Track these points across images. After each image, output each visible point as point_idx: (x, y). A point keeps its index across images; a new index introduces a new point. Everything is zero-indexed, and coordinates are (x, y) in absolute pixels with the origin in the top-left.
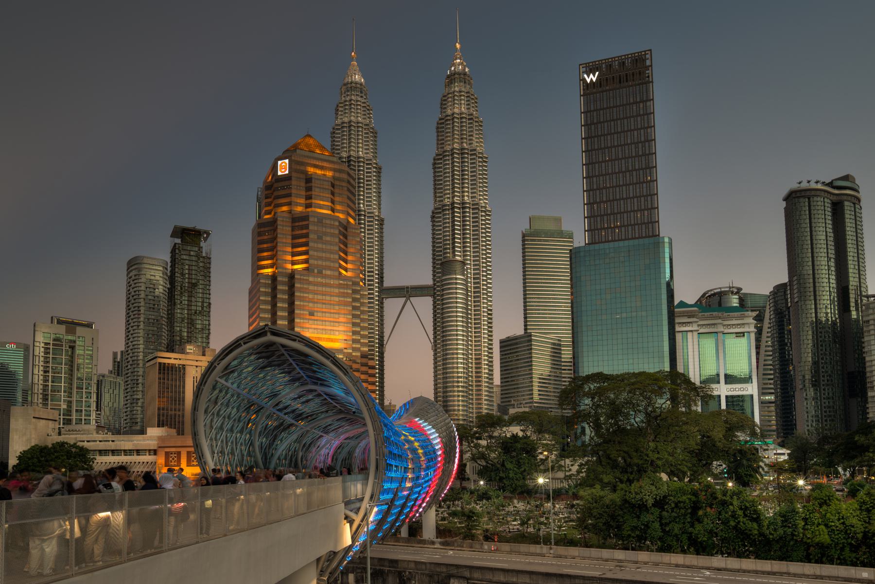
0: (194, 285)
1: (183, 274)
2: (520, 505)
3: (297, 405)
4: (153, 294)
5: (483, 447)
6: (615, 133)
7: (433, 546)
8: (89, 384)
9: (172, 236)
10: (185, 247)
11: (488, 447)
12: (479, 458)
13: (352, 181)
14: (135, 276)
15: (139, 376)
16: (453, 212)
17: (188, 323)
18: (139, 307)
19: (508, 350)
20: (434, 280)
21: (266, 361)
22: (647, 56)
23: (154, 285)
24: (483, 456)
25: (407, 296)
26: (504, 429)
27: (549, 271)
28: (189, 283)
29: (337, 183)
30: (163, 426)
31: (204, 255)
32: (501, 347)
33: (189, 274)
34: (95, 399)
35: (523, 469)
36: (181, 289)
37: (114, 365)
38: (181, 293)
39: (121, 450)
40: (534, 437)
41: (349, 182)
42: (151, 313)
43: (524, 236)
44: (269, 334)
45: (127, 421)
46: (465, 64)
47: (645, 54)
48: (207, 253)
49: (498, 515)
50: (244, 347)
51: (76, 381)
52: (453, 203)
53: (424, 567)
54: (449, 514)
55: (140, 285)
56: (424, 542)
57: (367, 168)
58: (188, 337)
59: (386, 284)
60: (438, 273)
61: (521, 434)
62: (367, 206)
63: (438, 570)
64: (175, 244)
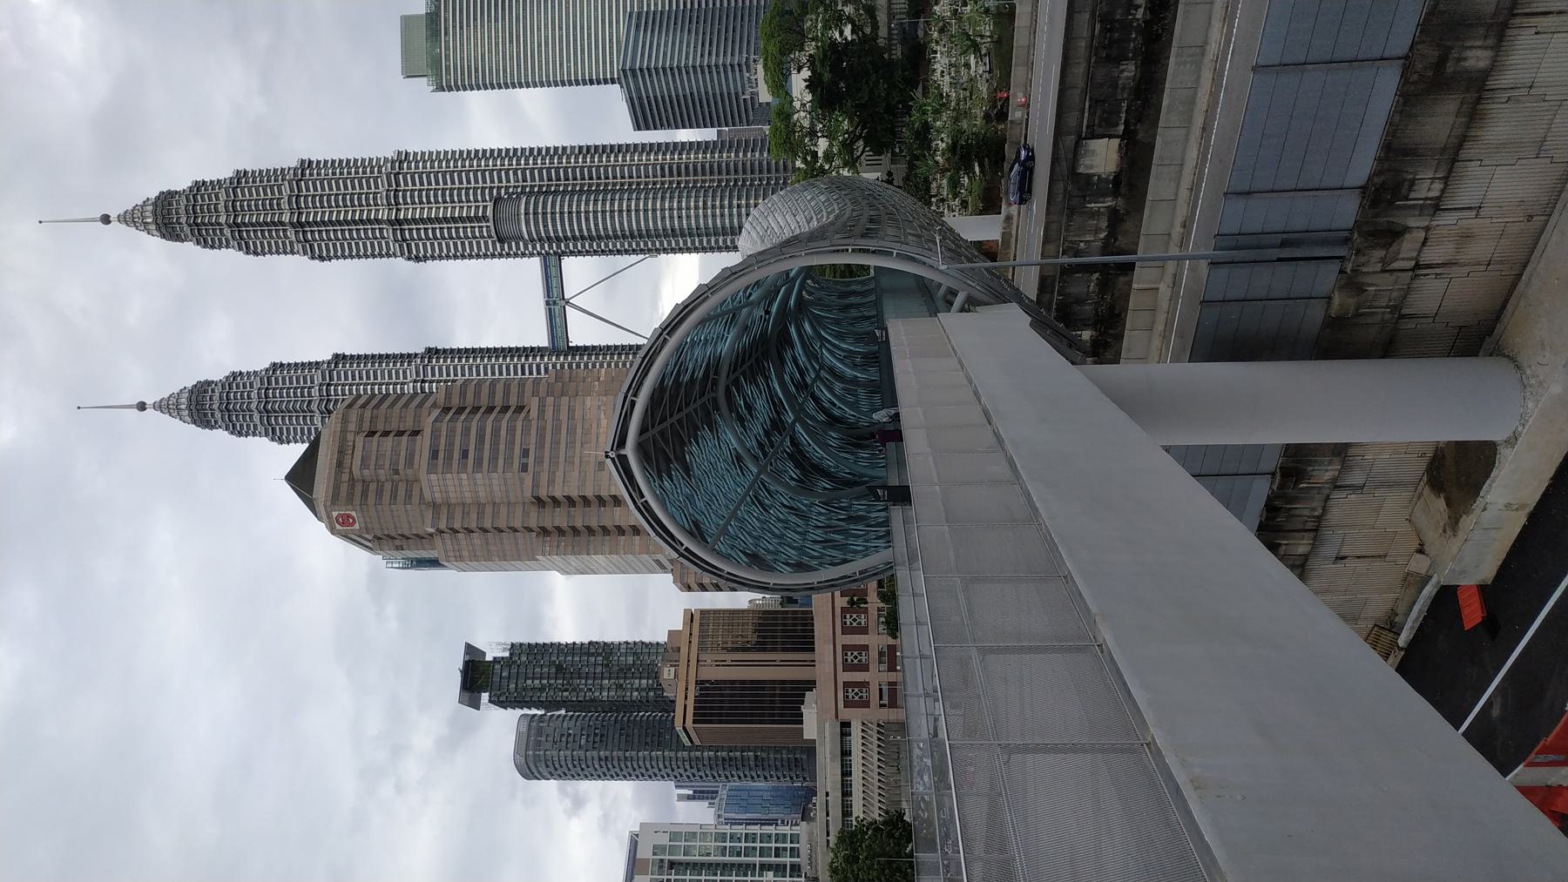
0: (559, 668)
1: (542, 689)
2: (940, 62)
3: (757, 429)
4: (577, 738)
5: (831, 145)
7: (1015, 218)
8: (731, 838)
9: (478, 708)
10: (496, 686)
11: (830, 136)
12: (852, 152)
13: (361, 402)
14: (548, 766)
16: (406, 221)
17: (625, 678)
18: (600, 759)
19: (652, 114)
20: (532, 255)
21: (675, 465)
23: (562, 735)
24: (848, 146)
25: (563, 303)
26: (797, 105)
27: (496, 10)
28: (556, 679)
29: (366, 427)
30: (801, 715)
31: (507, 654)
32: (648, 128)
33: (541, 678)
34: (758, 827)
35: (870, 67)
36: (566, 690)
37: (699, 798)
38: (574, 690)
39: (842, 781)
40: (811, 48)
41: (364, 406)
42: (610, 739)
43: (440, 88)
44: (622, 452)
48: (504, 650)
49: (958, 101)
50: (648, 497)
51: (727, 858)
52: (390, 222)
53: (1054, 226)
54: (955, 196)
55: (562, 758)
56: (1006, 236)
57: (277, 383)
58: (648, 678)
59: (543, 341)
60: (518, 248)
61: (806, 73)
62: (405, 378)
63: (1060, 198)
64: (490, 701)
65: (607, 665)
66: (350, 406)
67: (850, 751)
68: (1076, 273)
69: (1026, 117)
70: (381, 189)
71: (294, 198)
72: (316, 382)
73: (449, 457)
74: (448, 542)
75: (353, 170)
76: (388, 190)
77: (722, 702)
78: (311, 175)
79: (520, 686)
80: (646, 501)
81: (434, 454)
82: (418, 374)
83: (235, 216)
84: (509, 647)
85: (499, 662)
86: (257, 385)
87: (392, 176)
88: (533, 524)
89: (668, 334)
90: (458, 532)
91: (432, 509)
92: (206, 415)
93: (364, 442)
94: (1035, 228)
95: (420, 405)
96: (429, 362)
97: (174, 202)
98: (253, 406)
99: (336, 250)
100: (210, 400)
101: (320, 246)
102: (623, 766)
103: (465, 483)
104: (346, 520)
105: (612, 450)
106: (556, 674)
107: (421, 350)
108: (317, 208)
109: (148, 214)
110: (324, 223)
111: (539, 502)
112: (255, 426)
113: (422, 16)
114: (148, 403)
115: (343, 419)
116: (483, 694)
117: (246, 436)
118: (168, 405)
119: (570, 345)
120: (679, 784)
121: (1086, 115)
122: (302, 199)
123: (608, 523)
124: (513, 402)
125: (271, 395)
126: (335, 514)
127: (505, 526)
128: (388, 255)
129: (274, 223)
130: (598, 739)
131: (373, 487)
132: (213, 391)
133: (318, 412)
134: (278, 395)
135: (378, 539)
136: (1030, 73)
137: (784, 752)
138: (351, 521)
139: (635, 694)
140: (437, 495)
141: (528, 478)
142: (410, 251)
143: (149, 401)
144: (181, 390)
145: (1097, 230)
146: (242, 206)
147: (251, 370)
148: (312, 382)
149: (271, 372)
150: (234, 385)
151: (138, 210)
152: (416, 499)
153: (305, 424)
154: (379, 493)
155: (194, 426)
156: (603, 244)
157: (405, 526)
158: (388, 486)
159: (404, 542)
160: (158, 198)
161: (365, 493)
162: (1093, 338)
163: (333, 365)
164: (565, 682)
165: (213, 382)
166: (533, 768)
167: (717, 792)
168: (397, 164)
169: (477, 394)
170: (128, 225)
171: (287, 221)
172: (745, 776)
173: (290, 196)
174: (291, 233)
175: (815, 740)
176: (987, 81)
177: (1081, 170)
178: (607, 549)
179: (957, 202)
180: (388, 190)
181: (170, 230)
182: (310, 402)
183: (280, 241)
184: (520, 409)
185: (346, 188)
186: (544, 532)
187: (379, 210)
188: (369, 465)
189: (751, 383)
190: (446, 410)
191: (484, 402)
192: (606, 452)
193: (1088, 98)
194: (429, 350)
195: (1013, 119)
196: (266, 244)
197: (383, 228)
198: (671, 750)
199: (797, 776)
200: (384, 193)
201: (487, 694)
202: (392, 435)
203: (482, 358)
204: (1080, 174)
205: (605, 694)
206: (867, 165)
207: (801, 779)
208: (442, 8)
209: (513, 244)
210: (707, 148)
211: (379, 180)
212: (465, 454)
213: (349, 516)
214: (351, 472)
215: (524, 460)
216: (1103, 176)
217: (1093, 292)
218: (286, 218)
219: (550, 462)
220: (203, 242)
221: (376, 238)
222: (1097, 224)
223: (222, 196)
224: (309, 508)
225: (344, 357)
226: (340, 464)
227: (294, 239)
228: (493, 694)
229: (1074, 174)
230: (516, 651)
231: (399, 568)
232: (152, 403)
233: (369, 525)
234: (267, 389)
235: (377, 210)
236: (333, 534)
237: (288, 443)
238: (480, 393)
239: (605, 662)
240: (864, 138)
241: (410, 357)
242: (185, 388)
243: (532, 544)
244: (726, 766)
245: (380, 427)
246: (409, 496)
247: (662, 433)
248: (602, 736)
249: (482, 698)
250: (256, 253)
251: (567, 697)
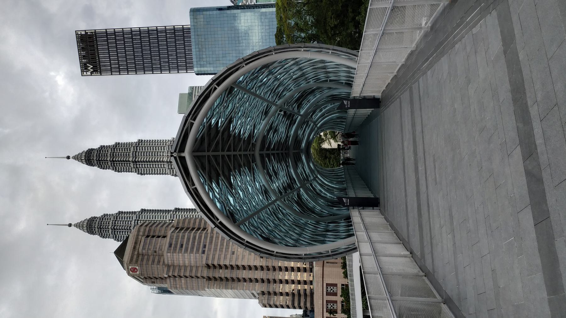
6: (125, 53)
13: (145, 224)
22: (79, 33)
29: (146, 233)
41: (146, 226)
44: (183, 155)
47: (78, 34)
57: (119, 219)
66: (141, 225)
70: (165, 150)
71: (135, 152)
72: (134, 219)
73: (176, 247)
74: (172, 281)
75: (162, 143)
76: (168, 151)
78: (142, 145)
81: (170, 245)
82: (171, 218)
86: (112, 219)
87: (135, 147)
88: (205, 275)
90: (182, 277)
91: (167, 267)
92: (92, 229)
93: (145, 239)
95: (167, 226)
96: (175, 213)
97: (93, 153)
98: (110, 227)
99: (147, 171)
100: (95, 224)
101: (141, 169)
103: (180, 257)
104: (134, 270)
105: (175, 151)
107: (173, 209)
108: (142, 156)
109: (83, 156)
110: (160, 161)
111: (214, 267)
112: (109, 235)
113: (187, 93)
114: (72, 224)
117: (106, 238)
118: (80, 225)
122: (137, 153)
123: (240, 277)
124: (202, 226)
125: (117, 223)
126: (130, 267)
127: (194, 275)
128: (165, 174)
129: (126, 161)
131: (146, 257)
132: (96, 221)
133: (110, 229)
134: (119, 223)
135: (146, 279)
138: (136, 270)
140: (170, 262)
141: (205, 256)
143: (73, 224)
144: (85, 220)
146: (116, 155)
147: (111, 213)
148: (132, 219)
149: (118, 215)
151: (80, 155)
152: (161, 263)
153: (123, 234)
154: (148, 260)
155: (87, 233)
157: (156, 273)
158: (151, 258)
159: (155, 280)
160: (87, 151)
161: (142, 260)
163: (140, 213)
165: (97, 217)
168: (172, 142)
169: (189, 222)
170: (75, 160)
171: (131, 160)
173: (133, 152)
174: (132, 165)
178: (230, 287)
181: (90, 162)
182: (130, 226)
183: (122, 167)
184: (204, 229)
185: (153, 149)
186: (209, 279)
187: (164, 158)
188: (145, 249)
190: (177, 228)
191: (191, 226)
194: (176, 209)
196: (122, 168)
197: (165, 164)
200: (167, 152)
202: (161, 237)
203: (192, 212)
208: (194, 91)
211: (165, 147)
212: (182, 246)
213: (136, 268)
214: (138, 251)
215: (204, 249)
218: (130, 159)
219: (225, 251)
220: (101, 167)
221: (148, 168)
223: (132, 149)
224: (121, 265)
225: (145, 210)
226: (134, 248)
227: (133, 167)
231: (156, 293)
232: (74, 224)
233: (143, 273)
234: (116, 221)
235: (163, 158)
236: (129, 275)
238: (190, 222)
241: (169, 211)
242: (86, 219)
243: (204, 283)
245: (152, 234)
246: (159, 262)
250: (119, 172)
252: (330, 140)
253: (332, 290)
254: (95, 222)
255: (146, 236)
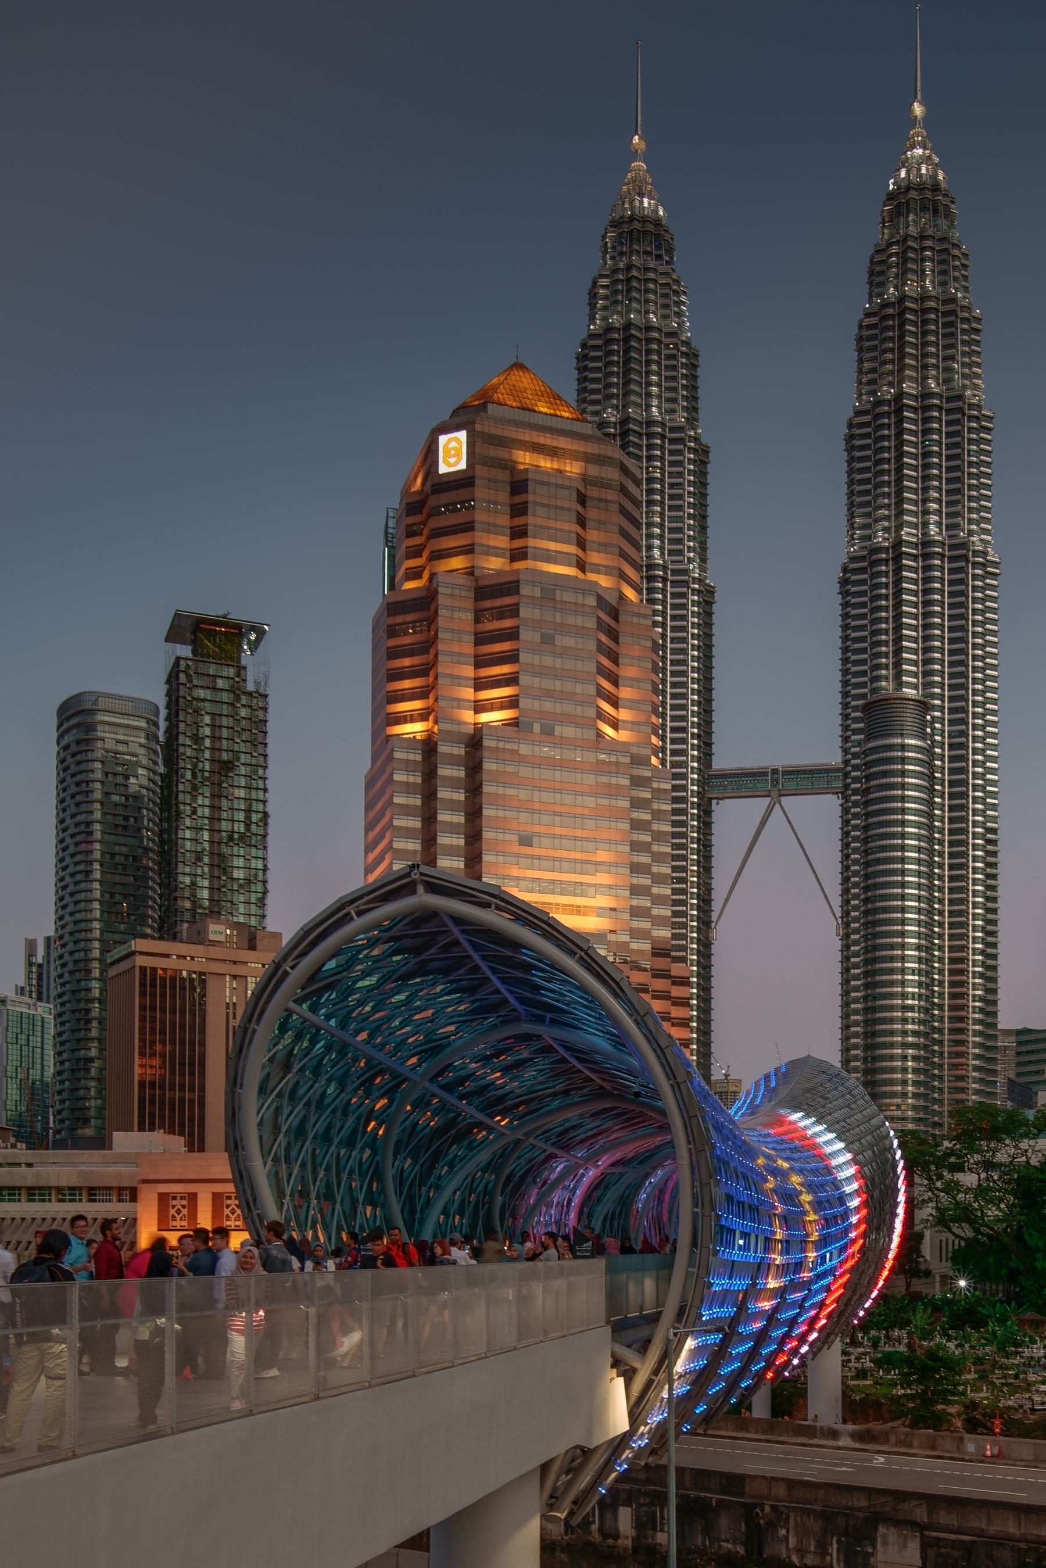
1: (197, 739)
7: (832, 1443)
9: (168, 639)
11: (980, 1191)
15: (92, 1000)
20: (845, 751)
24: (965, 1214)
26: (1024, 1144)
28: (212, 761)
29: (593, 492)
31: (250, 687)
38: (195, 788)
41: (624, 490)
42: (119, 839)
44: (420, 889)
45: (65, 998)
46: (936, 160)
48: (257, 683)
56: (811, 1431)
58: (211, 900)
59: (720, 762)
60: (855, 732)
64: (178, 659)
65: (231, 838)
67: (95, 1201)
68: (747, 1524)
69: (967, 1458)
77: (173, 1011)
79: (201, 705)
80: (352, 919)
83: (916, 311)
84: (262, 691)
85: (238, 675)
89: (581, 958)
94: (814, 1469)
102: (79, 858)
105: (422, 874)
106: (220, 762)
115: (605, 457)
116: (190, 648)
119: (714, 802)
120: (52, 941)
121: (953, 1537)
130: (120, 821)
136: (1023, 1463)
137: (99, 1102)
139: (187, 880)
142: (855, 571)
145: (801, 1552)
150: (667, 291)
156: (857, 856)
162: (658, 1547)
164: (207, 774)
166: (73, 722)
167: (40, 999)
172: (62, 1043)
175: (111, 1148)
176: (1021, 1406)
177: (882, 1530)
179: (869, 1364)
180: (943, 544)
189: (552, 1069)
192: (418, 866)
193: (975, 1538)
195: (965, 1441)
198: (102, 932)
199: (62, 1121)
201: (190, 655)
204: (876, 1528)
205: (188, 834)
206: (941, 1241)
207: (58, 1127)
209: (862, 725)
210: (988, 1014)
216: (872, 1560)
217: (720, 1547)
222: (810, 1552)
228: (190, 663)
229: (877, 1519)
230: (255, 701)
231: (387, 527)
237: (578, 369)
239: (236, 836)
240: (975, 1239)
244: (77, 1015)
245: (591, 514)
247: (456, 943)
248: (125, 827)
249: (184, 646)
251: (183, 777)
252: (933, 1204)
253: (179, 1212)
254: (651, 253)
255: (583, 491)
